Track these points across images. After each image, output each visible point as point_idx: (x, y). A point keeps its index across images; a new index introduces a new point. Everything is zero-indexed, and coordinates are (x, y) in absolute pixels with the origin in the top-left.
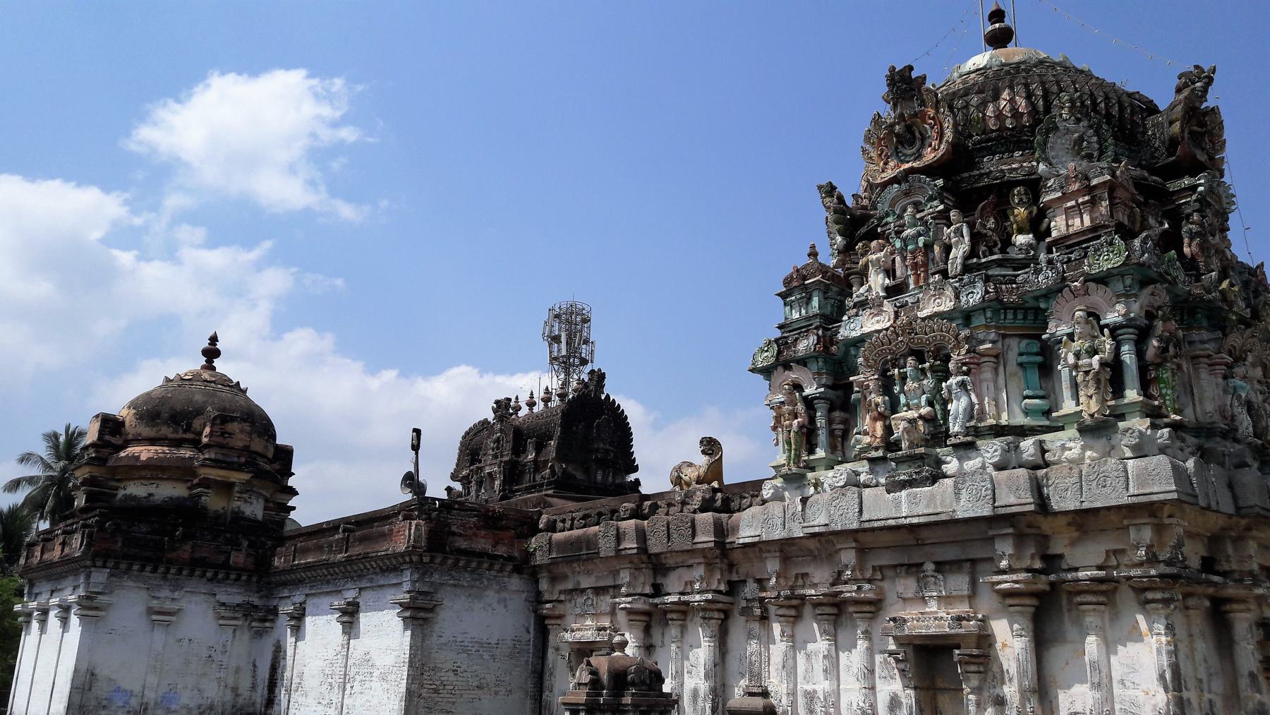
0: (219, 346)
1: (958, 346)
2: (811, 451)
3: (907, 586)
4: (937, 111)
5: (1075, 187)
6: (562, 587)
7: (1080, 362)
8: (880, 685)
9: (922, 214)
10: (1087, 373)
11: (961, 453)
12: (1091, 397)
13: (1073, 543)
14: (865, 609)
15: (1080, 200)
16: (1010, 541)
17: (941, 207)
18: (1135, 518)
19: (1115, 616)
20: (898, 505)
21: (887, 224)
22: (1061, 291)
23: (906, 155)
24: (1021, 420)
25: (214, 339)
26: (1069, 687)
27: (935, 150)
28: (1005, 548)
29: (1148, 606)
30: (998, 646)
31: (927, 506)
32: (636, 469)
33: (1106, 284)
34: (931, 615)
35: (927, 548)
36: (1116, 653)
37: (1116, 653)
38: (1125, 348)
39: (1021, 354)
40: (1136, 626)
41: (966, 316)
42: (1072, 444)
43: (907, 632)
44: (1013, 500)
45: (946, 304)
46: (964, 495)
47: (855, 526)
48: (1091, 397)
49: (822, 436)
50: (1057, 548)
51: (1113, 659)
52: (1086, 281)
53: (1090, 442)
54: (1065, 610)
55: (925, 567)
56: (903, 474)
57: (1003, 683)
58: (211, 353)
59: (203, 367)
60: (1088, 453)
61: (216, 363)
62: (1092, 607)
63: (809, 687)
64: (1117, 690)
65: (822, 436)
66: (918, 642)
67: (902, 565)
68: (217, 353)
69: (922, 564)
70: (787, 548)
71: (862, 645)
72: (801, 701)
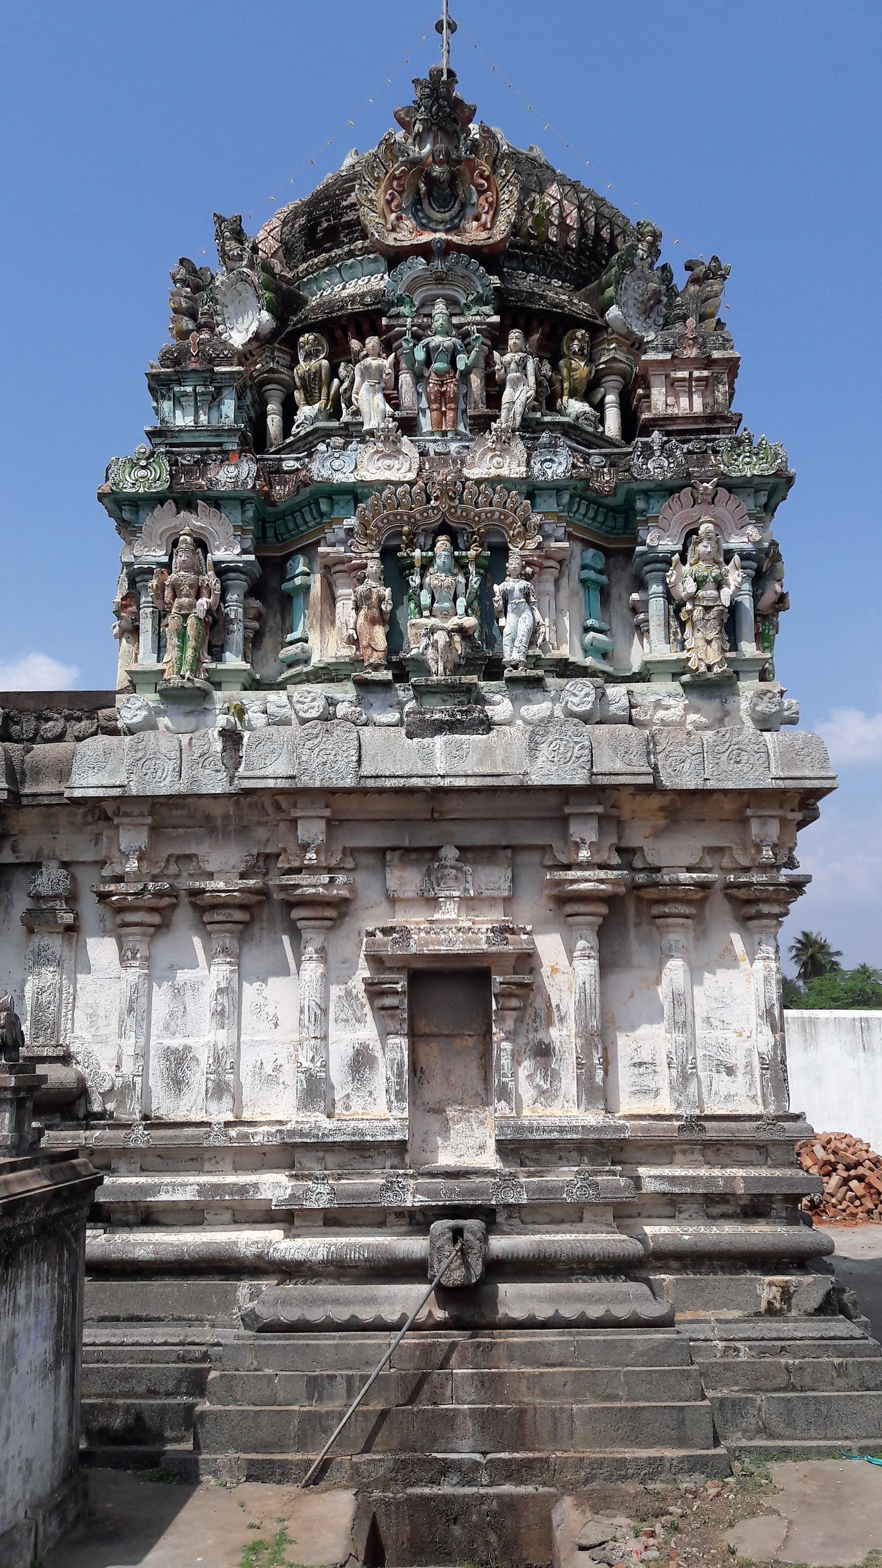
1: (525, 533)
2: (217, 657)
3: (406, 880)
4: (494, 170)
5: (693, 353)
7: (701, 593)
8: (335, 1032)
9: (462, 320)
10: (707, 609)
11: (519, 691)
12: (709, 642)
13: (657, 834)
14: (319, 913)
15: (696, 374)
16: (594, 823)
17: (496, 319)
18: (763, 808)
19: (702, 933)
20: (428, 756)
21: (398, 316)
22: (680, 489)
23: (430, 219)
24: (578, 658)
26: (633, 1028)
27: (484, 228)
28: (585, 832)
29: (752, 924)
30: (545, 971)
31: (481, 762)
33: (217, 507)
34: (452, 924)
35: (445, 826)
36: (701, 983)
37: (701, 983)
38: (233, 597)
39: (584, 567)
40: (729, 947)
41: (532, 490)
42: (671, 702)
43: (414, 949)
44: (619, 766)
45: (512, 467)
46: (544, 751)
47: (349, 782)
48: (709, 642)
49: (237, 635)
50: (635, 838)
51: (696, 989)
52: (718, 485)
53: (698, 702)
54: (631, 923)
55: (443, 853)
56: (439, 711)
57: (550, 1023)
60: (692, 717)
62: (681, 921)
63: (176, 1042)
64: (700, 1030)
65: (237, 635)
66: (419, 965)
67: (394, 849)
69: (438, 849)
70: (165, 812)
71: (312, 970)
72: (156, 1065)
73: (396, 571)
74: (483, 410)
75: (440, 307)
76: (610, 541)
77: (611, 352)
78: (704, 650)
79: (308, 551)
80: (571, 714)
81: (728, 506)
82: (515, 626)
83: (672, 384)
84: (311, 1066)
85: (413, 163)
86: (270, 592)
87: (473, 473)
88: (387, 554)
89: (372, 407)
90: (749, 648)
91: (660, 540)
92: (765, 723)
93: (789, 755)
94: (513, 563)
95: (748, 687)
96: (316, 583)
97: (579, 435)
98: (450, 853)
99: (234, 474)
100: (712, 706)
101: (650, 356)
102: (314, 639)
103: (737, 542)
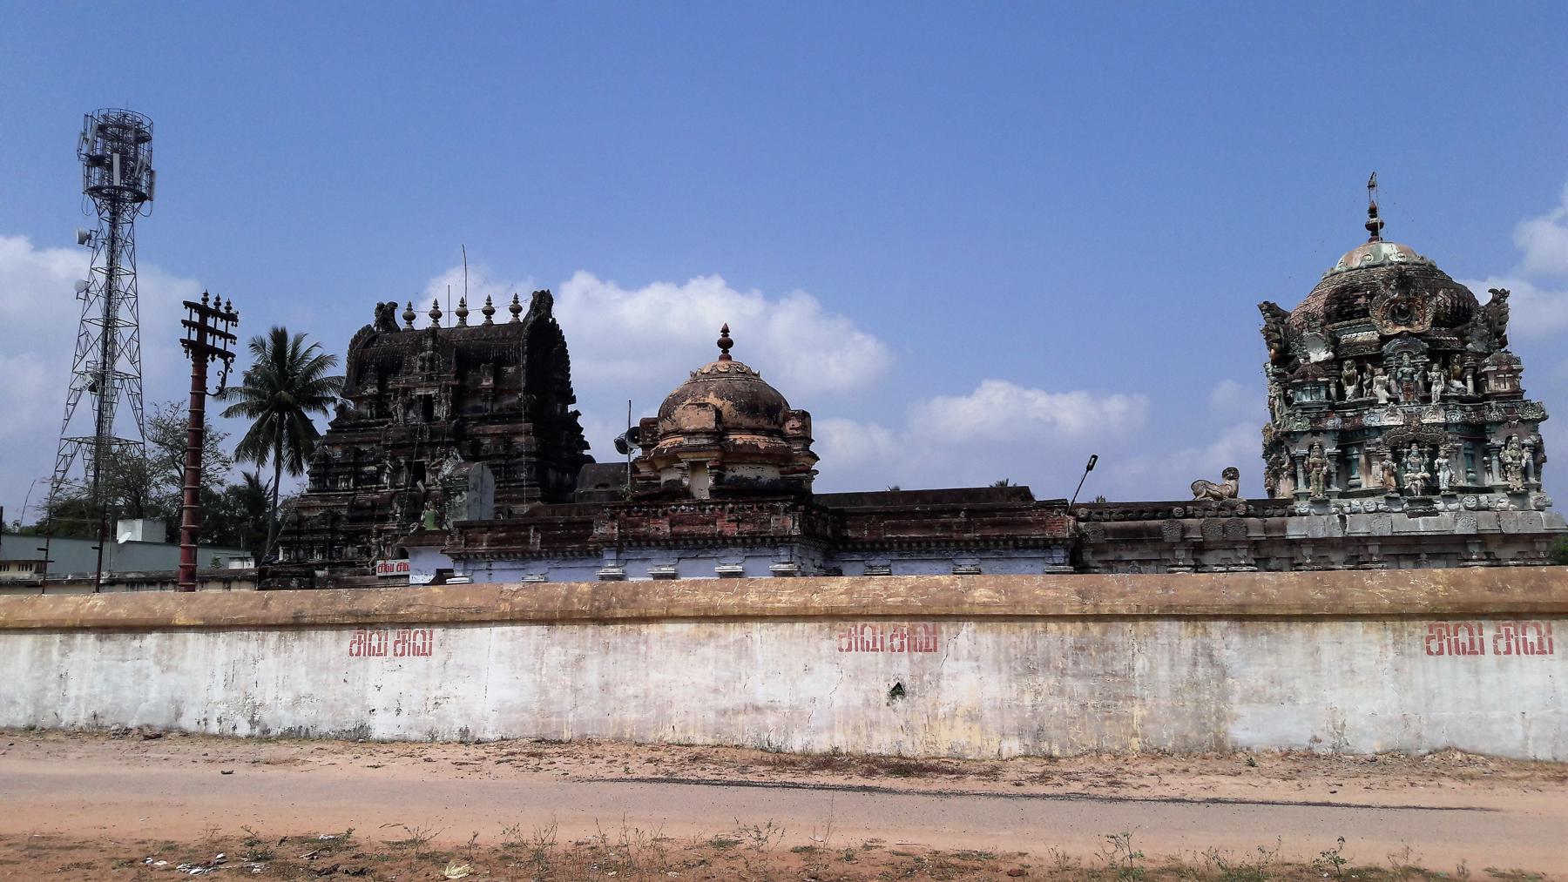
0: (731, 336)
6: (1102, 558)
13: (1499, 547)
20: (1417, 524)
25: (725, 331)
32: (573, 400)
45: (1440, 419)
46: (1460, 523)
58: (725, 344)
59: (721, 358)
61: (731, 351)
68: (730, 343)
73: (1397, 457)
74: (1424, 394)
75: (1406, 356)
76: (1476, 439)
77: (1469, 361)
78: (1515, 482)
79: (1359, 446)
80: (1467, 509)
81: (1522, 429)
82: (1443, 476)
83: (1497, 380)
84: (854, 738)
85: (1392, 301)
86: (1345, 463)
87: (1425, 421)
88: (1393, 450)
89: (1382, 395)
90: (1532, 480)
91: (1496, 441)
92: (1540, 509)
93: (1550, 521)
94: (1442, 453)
95: (1533, 495)
96: (1363, 459)
97: (1463, 400)
98: (1424, 556)
99: (1333, 422)
100: (1519, 502)
101: (1487, 369)
102: (1363, 479)
103: (1526, 441)
